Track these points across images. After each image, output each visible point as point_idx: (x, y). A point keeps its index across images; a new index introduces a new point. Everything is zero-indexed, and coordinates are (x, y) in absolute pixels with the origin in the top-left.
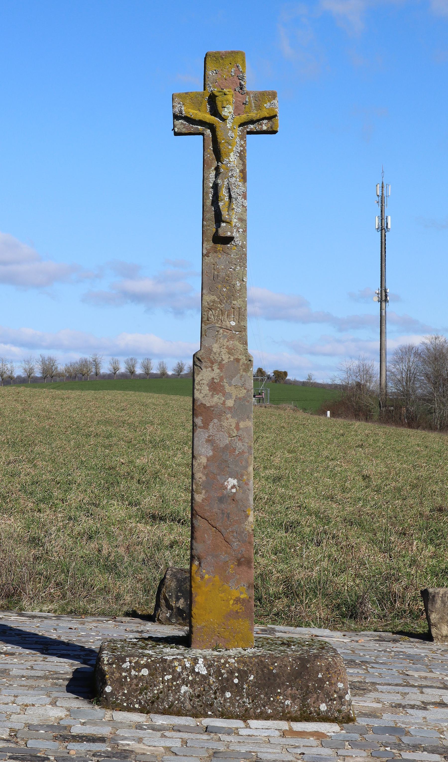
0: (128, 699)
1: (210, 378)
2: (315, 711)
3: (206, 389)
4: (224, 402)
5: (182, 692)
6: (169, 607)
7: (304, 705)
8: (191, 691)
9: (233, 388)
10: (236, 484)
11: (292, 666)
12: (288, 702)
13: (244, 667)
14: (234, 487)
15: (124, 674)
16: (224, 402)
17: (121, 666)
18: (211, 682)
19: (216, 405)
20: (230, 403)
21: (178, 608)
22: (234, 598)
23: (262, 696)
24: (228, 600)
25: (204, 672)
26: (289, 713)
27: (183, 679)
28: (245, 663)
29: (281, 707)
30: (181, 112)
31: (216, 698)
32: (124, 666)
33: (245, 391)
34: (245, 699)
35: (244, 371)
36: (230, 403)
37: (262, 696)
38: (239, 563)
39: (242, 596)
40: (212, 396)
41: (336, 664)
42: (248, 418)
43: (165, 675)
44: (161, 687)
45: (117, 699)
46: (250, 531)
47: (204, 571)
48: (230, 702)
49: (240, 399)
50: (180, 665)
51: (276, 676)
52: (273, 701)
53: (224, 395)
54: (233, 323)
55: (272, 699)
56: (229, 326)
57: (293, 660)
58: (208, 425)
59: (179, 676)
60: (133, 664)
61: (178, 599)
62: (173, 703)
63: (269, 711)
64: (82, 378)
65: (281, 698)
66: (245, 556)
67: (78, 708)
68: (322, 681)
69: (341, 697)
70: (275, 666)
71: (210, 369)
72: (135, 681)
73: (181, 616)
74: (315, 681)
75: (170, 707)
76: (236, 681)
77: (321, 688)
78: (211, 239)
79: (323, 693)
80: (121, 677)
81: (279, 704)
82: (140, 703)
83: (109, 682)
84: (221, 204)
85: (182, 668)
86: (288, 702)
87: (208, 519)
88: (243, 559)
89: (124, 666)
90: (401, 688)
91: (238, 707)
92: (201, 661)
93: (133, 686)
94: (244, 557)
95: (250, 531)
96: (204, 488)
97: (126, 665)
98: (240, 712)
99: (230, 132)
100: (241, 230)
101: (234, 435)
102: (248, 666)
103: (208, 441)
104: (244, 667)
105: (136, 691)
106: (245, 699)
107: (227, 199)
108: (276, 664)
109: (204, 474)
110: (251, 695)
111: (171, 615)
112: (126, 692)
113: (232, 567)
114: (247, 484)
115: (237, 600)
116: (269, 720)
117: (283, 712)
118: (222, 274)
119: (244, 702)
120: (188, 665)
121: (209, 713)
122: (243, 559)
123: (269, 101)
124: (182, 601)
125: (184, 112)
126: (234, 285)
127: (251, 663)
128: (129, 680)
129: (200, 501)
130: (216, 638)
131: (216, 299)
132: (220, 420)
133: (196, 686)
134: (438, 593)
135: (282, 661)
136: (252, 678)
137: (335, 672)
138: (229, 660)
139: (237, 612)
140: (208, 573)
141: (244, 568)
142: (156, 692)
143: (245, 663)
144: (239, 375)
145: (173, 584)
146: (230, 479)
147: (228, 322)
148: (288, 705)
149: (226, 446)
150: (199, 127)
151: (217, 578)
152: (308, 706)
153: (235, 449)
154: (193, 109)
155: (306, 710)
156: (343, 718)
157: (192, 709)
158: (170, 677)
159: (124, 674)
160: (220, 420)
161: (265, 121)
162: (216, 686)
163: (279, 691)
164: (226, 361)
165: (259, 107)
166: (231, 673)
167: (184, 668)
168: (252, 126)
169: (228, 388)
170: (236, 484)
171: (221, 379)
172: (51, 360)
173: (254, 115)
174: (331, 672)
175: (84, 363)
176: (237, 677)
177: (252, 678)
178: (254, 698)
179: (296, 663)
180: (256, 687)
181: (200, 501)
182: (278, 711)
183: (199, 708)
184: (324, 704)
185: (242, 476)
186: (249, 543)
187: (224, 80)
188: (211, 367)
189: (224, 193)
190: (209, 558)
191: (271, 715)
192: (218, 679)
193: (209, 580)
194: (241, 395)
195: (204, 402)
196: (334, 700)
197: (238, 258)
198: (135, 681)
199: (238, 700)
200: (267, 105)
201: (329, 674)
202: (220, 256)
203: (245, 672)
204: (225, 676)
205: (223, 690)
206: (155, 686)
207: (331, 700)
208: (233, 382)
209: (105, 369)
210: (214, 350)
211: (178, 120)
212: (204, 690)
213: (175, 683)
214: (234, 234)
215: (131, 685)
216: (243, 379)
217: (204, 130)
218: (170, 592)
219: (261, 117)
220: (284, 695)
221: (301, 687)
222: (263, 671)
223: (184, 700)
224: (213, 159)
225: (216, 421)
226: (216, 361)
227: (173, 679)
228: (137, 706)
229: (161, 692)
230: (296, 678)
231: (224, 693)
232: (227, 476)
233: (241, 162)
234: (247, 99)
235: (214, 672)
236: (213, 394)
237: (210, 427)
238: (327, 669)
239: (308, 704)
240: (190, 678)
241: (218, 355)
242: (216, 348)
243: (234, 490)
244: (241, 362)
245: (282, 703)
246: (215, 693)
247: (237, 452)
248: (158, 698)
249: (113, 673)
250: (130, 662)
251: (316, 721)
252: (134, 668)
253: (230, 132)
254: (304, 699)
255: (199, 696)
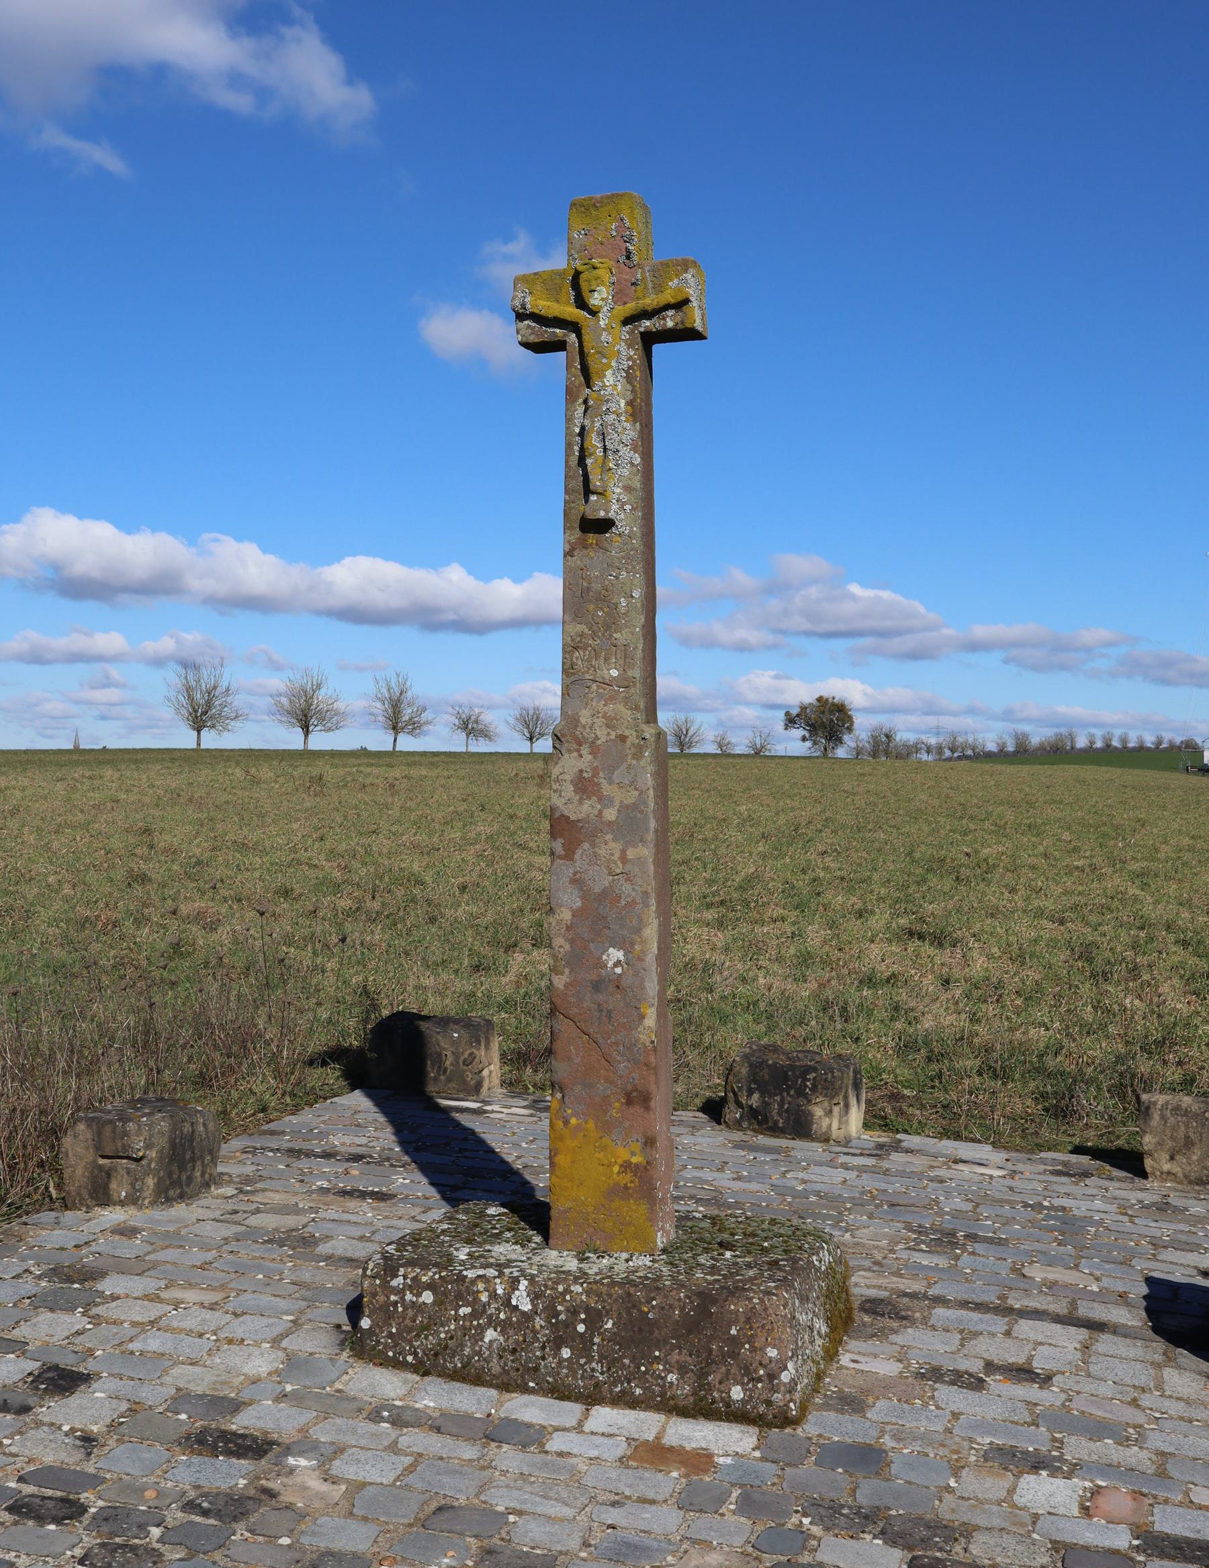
0: (396, 1345)
1: (576, 770)
2: (722, 1399)
3: (569, 790)
4: (600, 812)
5: (487, 1340)
6: (739, 1104)
7: (701, 1385)
8: (502, 1339)
9: (615, 787)
10: (622, 958)
11: (682, 1309)
12: (672, 1377)
13: (597, 1302)
14: (618, 963)
15: (393, 1298)
16: (600, 812)
17: (388, 1282)
18: (538, 1327)
19: (587, 820)
20: (610, 814)
21: (751, 1107)
22: (620, 1161)
23: (626, 1361)
24: (610, 1165)
25: (526, 1306)
26: (673, 1397)
27: (491, 1316)
28: (599, 1295)
29: (658, 1385)
30: (523, 306)
31: (543, 1358)
32: (394, 1283)
33: (637, 793)
34: (594, 1365)
35: (633, 758)
36: (610, 814)
37: (626, 1361)
38: (629, 1102)
39: (634, 1160)
40: (580, 802)
41: (766, 1309)
42: (641, 841)
43: (461, 1306)
44: (452, 1327)
45: (378, 1342)
46: (648, 1043)
47: (569, 1111)
48: (568, 1368)
49: (627, 807)
50: (486, 1290)
51: (653, 1324)
52: (646, 1372)
53: (600, 800)
54: (614, 673)
55: (643, 1368)
56: (607, 677)
57: (687, 1297)
58: (574, 853)
59: (484, 1311)
60: (408, 1281)
61: (750, 1093)
62: (470, 1358)
63: (638, 1391)
64: (1058, 753)
65: (661, 1367)
66: (639, 1088)
67: (311, 1354)
68: (735, 1342)
69: (772, 1376)
70: (653, 1307)
71: (575, 754)
72: (410, 1313)
73: (756, 1118)
74: (723, 1342)
75: (463, 1367)
76: (581, 1328)
77: (734, 1355)
78: (577, 525)
79: (738, 1365)
80: (388, 1303)
81: (656, 1379)
82: (415, 1354)
83: (367, 1312)
84: (589, 461)
85: (490, 1297)
86: (672, 1377)
87: (576, 1019)
88: (635, 1094)
89: (394, 1283)
90: (976, 1316)
91: (583, 1378)
92: (523, 1284)
93: (407, 1322)
94: (637, 1090)
95: (648, 1043)
96: (568, 964)
97: (397, 1282)
98: (585, 1387)
99: (605, 334)
100: (628, 507)
101: (618, 871)
102: (604, 1301)
103: (574, 881)
104: (597, 1302)
105: (410, 1330)
106: (594, 1365)
107: (599, 453)
108: (654, 1303)
109: (567, 940)
110: (606, 1358)
111: (741, 1116)
112: (394, 1330)
113: (616, 1108)
114: (640, 959)
115: (627, 1166)
116: (634, 1408)
117: (663, 1394)
118: (596, 586)
119: (593, 1370)
120: (500, 1291)
121: (531, 1384)
122: (635, 1094)
123: (677, 276)
124: (756, 1096)
125: (528, 306)
126: (616, 606)
127: (610, 1296)
128: (400, 1309)
129: (561, 987)
130: (591, 1230)
131: (586, 631)
132: (593, 846)
133: (511, 1332)
134: (1155, 1103)
135: (666, 1297)
136: (609, 1325)
137: (763, 1326)
138: (572, 1288)
139: (626, 1187)
140: (575, 1114)
141: (637, 1109)
142: (443, 1336)
143: (599, 1295)
144: (625, 765)
145: (744, 1071)
146: (611, 950)
147: (605, 672)
148: (672, 1383)
149: (605, 890)
150: (558, 331)
151: (591, 1125)
152: (710, 1388)
153: (619, 898)
154: (547, 299)
155: (705, 1396)
156: (775, 1417)
157: (501, 1374)
158: (468, 1310)
159: (393, 1298)
160: (593, 846)
161: (670, 313)
162: (546, 1335)
163: (657, 1353)
164: (603, 739)
165: (659, 288)
166: (573, 1312)
167: (493, 1295)
168: (648, 323)
169: (606, 789)
170: (622, 958)
171: (595, 771)
172: (1025, 736)
173: (651, 301)
174: (755, 1326)
175: (1060, 737)
176: (583, 1321)
177: (609, 1325)
178: (611, 1362)
179: (692, 1302)
180: (616, 1343)
181: (561, 987)
182: (654, 1392)
183: (513, 1374)
184: (739, 1388)
185: (632, 944)
186: (646, 1065)
187: (599, 246)
188: (578, 751)
189: (594, 441)
190: (578, 1089)
191: (642, 1398)
192: (550, 1322)
193: (578, 1126)
194: (630, 801)
195: (566, 813)
196: (759, 1380)
197: (623, 558)
198: (410, 1313)
199: (582, 1366)
200: (674, 283)
201: (751, 1329)
202: (592, 554)
203: (599, 1313)
204: (562, 1317)
205: (558, 1344)
206: (443, 1325)
207: (753, 1379)
208: (616, 777)
209: (1081, 742)
210: (583, 721)
211: (521, 321)
212: (524, 1341)
213: (475, 1323)
214: (611, 515)
215: (404, 1319)
216: (632, 772)
217: (565, 335)
218: (739, 1081)
219: (661, 304)
220: (667, 1362)
221: (698, 1351)
222: (629, 1313)
223: (490, 1355)
224: (580, 385)
225: (586, 846)
226: (586, 740)
227: (474, 1315)
228: (410, 1359)
229: (451, 1338)
230: (690, 1332)
231: (559, 1348)
232: (607, 945)
233: (629, 387)
234: (639, 276)
235: (544, 1308)
236: (581, 798)
237: (577, 857)
238: (748, 1321)
239: (709, 1384)
240: (502, 1316)
241: (588, 730)
242: (585, 717)
243: (618, 970)
244: (629, 742)
245: (662, 1378)
246: (543, 1348)
247: (623, 903)
248: (446, 1347)
249: (374, 1295)
250: (405, 1277)
251: (720, 1420)
252: (411, 1288)
253: (605, 334)
254: (702, 1375)
255: (514, 1351)
